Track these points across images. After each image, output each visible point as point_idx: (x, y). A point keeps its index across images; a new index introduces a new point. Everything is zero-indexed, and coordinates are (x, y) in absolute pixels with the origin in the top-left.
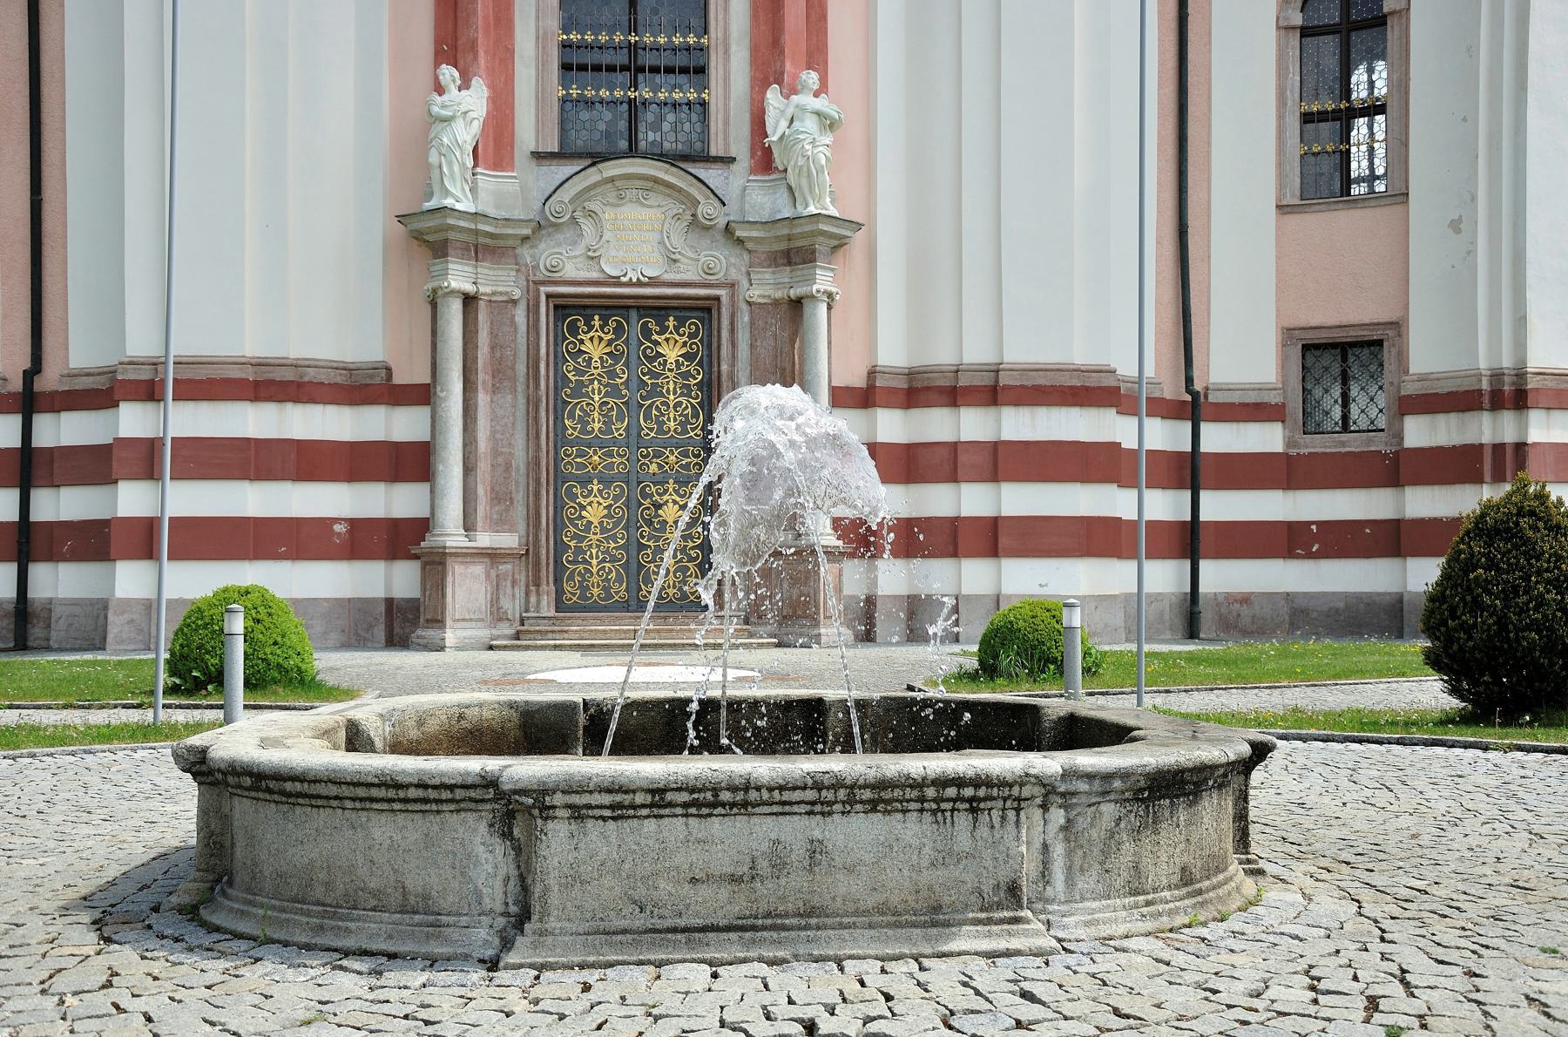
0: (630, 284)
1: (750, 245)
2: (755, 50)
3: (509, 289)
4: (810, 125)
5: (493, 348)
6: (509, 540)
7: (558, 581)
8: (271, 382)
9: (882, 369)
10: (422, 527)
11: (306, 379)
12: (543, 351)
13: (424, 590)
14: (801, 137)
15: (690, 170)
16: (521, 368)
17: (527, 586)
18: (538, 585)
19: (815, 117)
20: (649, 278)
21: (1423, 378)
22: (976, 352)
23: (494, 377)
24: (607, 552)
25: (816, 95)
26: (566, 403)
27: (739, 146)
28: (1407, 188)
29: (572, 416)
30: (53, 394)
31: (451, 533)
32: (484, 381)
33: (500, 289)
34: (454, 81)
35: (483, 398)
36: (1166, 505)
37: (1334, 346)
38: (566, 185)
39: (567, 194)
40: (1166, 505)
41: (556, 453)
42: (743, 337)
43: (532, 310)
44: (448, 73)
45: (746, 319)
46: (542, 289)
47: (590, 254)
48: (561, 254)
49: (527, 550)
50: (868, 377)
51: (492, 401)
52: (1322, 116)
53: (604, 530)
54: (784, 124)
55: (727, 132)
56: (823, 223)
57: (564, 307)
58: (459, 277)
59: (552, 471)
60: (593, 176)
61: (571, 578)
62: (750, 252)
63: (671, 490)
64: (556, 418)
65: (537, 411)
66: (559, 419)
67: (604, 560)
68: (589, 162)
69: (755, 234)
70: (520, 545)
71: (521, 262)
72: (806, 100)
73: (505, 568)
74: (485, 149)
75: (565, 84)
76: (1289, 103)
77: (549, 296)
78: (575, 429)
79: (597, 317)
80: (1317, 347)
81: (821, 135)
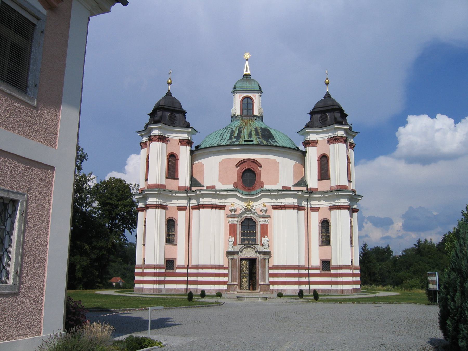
21: (333, 265)
25: (267, 238)
27: (259, 243)
30: (191, 267)
43: (238, 260)
44: (230, 237)
46: (240, 258)
54: (263, 241)
56: (307, 130)
72: (265, 238)
75: (242, 237)
77: (240, 259)
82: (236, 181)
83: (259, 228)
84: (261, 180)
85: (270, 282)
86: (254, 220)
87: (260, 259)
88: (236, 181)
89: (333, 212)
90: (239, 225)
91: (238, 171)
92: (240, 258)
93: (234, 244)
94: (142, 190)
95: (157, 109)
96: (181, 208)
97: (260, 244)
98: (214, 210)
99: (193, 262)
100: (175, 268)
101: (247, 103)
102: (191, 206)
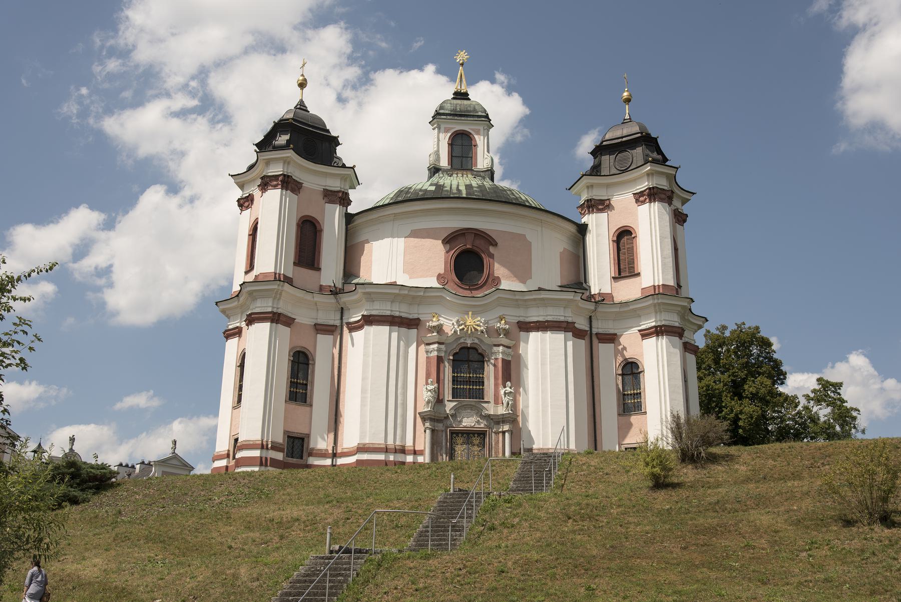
77: (450, 430)
82: (442, 272)
86: (479, 351)
88: (442, 272)
94: (242, 284)
95: (280, 126)
96: (328, 328)
100: (305, 455)
101: (462, 145)
102: (419, 413)
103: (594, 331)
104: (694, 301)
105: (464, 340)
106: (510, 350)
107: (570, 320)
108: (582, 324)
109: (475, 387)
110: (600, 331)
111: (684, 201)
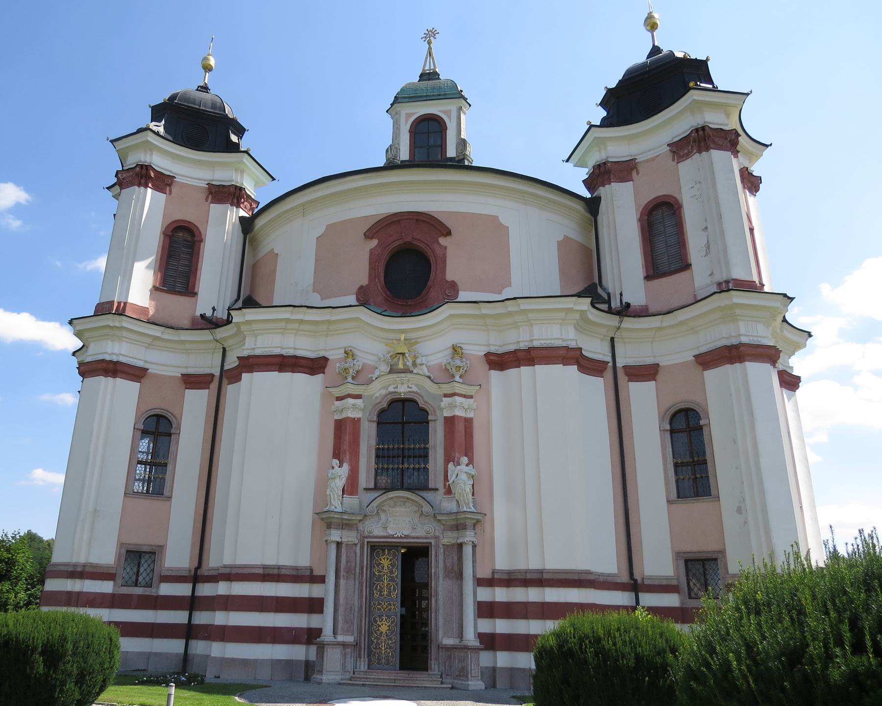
0: (398, 537)
1: (443, 522)
2: (446, 449)
3: (353, 540)
4: (463, 477)
5: (347, 562)
6: (350, 639)
7: (369, 656)
8: (269, 575)
9: (497, 571)
10: (319, 632)
11: (282, 573)
12: (365, 563)
13: (317, 658)
14: (460, 482)
15: (419, 494)
16: (358, 570)
17: (357, 658)
18: (360, 658)
19: (465, 474)
20: (405, 535)
22: (534, 564)
23: (347, 573)
24: (388, 644)
25: (467, 465)
26: (373, 583)
27: (440, 485)
28: (172, 494)
29: (376, 588)
31: (327, 635)
32: (343, 576)
33: (350, 540)
34: (337, 464)
35: (342, 582)
36: (202, 618)
37: (698, 560)
38: (375, 501)
39: (375, 504)
40: (202, 618)
41: (370, 604)
42: (441, 557)
43: (362, 548)
44: (336, 462)
45: (442, 550)
46: (366, 540)
47: (383, 526)
48: (373, 526)
49: (357, 643)
50: (492, 574)
51: (346, 583)
52: (683, 464)
53: (387, 635)
55: (435, 479)
57: (374, 546)
58: (335, 535)
59: (367, 610)
60: (384, 497)
61: (374, 655)
62: (444, 525)
63: (384, 619)
64: (370, 589)
65: (362, 586)
66: (371, 590)
67: (387, 648)
68: (384, 491)
69: (444, 518)
70: (354, 641)
71: (359, 529)
72: (463, 467)
73: (349, 650)
74: (347, 488)
76: (668, 459)
77: (368, 542)
78: (377, 594)
79: (386, 550)
80: (691, 560)
81: (468, 480)
83: (437, 435)
84: (449, 276)
85: (481, 636)
87: (443, 545)
89: (711, 375)
90: (367, 423)
91: (372, 252)
92: (366, 540)
93: (350, 488)
97: (442, 490)
98: (287, 377)
99: (213, 562)
103: (620, 363)
104: (792, 299)
105: (394, 388)
106: (471, 401)
107: (573, 345)
108: (597, 350)
109: (391, 466)
110: (631, 362)
111: (754, 157)
